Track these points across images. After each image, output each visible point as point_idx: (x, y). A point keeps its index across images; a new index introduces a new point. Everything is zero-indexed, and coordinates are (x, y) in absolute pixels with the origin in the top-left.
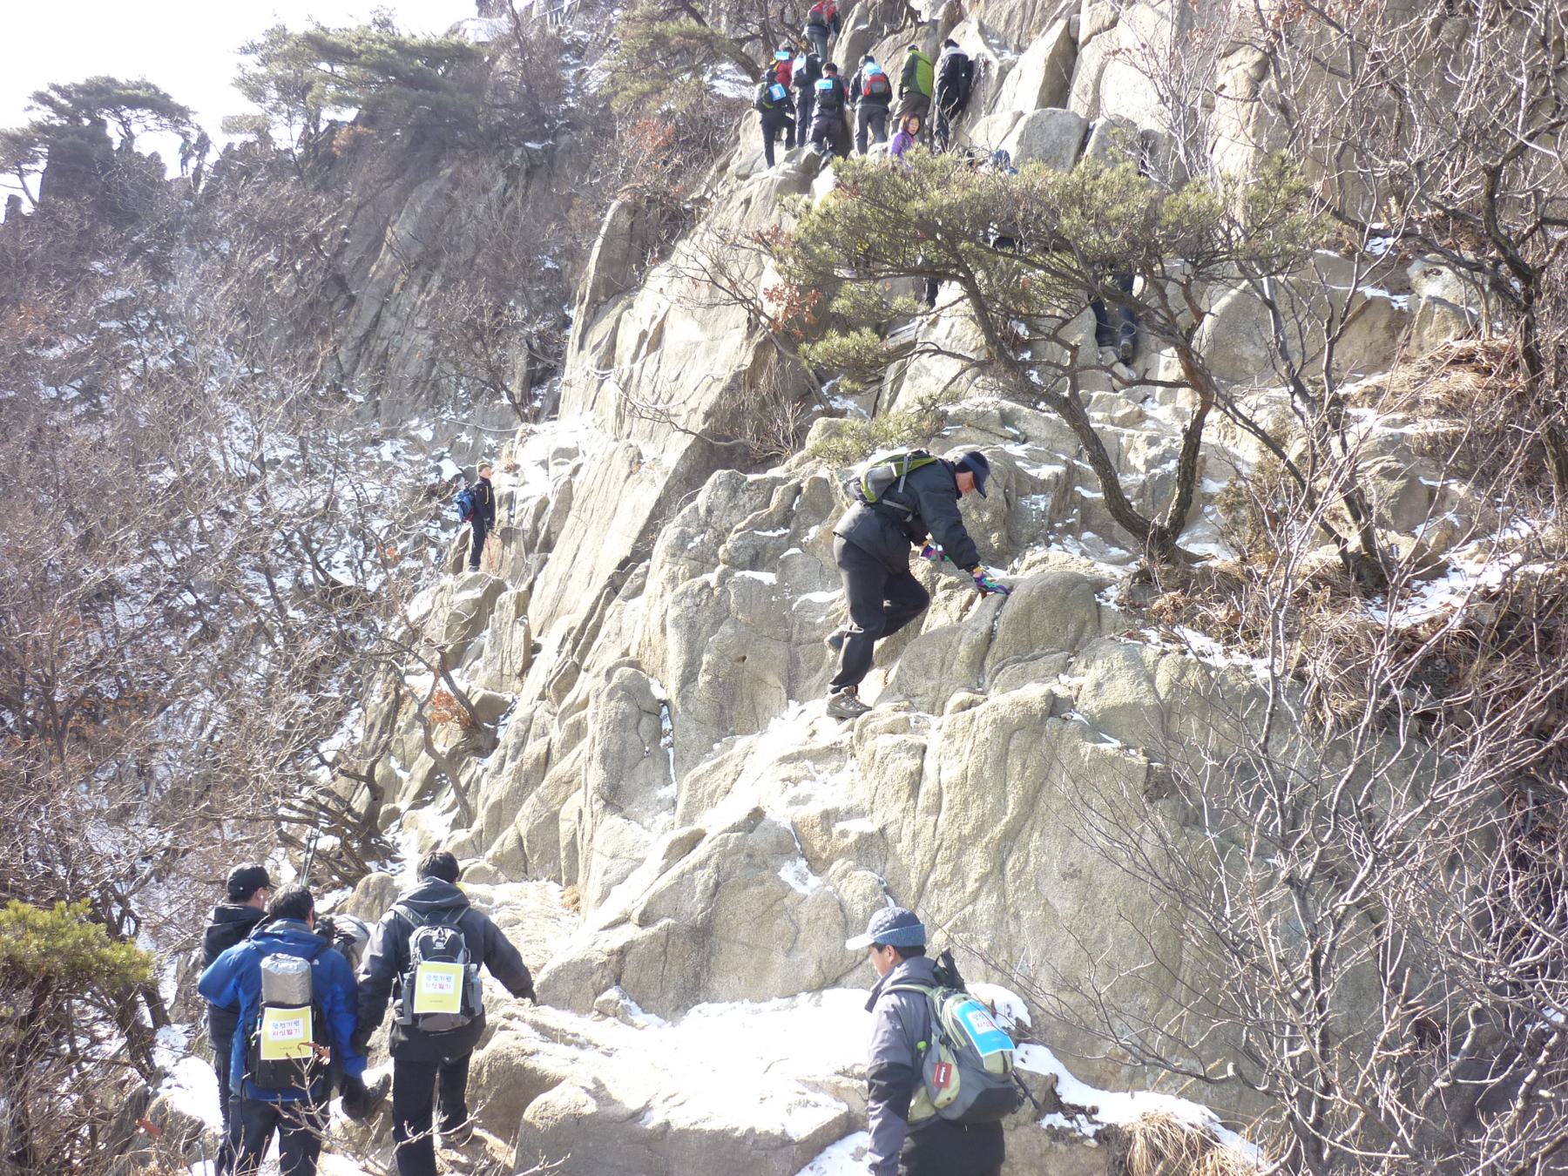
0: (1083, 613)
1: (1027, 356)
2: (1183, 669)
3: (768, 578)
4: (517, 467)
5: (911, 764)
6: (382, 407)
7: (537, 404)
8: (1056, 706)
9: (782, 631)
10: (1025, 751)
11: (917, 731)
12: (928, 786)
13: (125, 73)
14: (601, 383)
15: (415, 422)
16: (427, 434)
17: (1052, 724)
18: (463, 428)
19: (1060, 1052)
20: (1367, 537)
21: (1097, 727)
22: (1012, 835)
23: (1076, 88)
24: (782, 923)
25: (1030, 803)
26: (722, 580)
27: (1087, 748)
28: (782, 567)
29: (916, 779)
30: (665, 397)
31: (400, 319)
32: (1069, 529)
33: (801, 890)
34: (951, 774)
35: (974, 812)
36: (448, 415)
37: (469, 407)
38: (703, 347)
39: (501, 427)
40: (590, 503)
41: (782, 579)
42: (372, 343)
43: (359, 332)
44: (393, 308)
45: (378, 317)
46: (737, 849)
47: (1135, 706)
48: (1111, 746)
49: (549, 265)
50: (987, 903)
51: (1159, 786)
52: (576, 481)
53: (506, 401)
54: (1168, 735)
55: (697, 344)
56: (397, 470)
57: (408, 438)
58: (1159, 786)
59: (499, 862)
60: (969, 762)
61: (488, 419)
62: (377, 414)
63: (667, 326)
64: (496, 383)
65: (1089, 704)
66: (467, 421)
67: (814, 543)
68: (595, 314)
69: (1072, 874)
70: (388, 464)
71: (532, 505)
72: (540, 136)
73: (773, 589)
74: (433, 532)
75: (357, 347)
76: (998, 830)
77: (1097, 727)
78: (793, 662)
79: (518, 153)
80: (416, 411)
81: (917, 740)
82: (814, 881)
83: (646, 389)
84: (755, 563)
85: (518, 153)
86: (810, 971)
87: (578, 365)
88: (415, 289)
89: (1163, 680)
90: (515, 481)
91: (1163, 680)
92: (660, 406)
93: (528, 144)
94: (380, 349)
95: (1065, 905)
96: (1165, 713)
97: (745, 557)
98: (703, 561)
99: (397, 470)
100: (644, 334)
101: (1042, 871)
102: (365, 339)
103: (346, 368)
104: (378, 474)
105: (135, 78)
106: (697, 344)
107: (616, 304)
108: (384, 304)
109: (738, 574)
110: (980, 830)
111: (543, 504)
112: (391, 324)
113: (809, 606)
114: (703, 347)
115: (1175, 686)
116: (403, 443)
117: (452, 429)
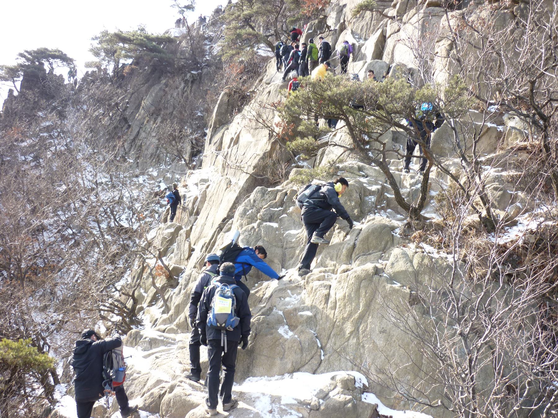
0: (387, 238)
1: (368, 147)
2: (423, 258)
3: (275, 225)
4: (187, 185)
5: (326, 292)
6: (139, 164)
7: (194, 163)
8: (377, 271)
9: (280, 244)
10: (366, 287)
11: (328, 280)
12: (331, 299)
13: (51, 47)
14: (217, 156)
15: (151, 169)
16: (155, 174)
17: (376, 278)
18: (168, 172)
19: (379, 396)
20: (488, 210)
21: (392, 279)
22: (362, 318)
23: (385, 53)
24: (279, 349)
25: (368, 306)
26: (259, 226)
27: (388, 286)
28: (280, 221)
29: (327, 297)
30: (239, 161)
31: (146, 133)
32: (382, 208)
33: (286, 337)
34: (340, 295)
35: (348, 309)
36: (163, 167)
37: (170, 164)
38: (253, 143)
39: (181, 171)
40: (213, 198)
41: (280, 226)
42: (136, 141)
43: (132, 138)
44: (144, 129)
45: (138, 132)
46: (263, 322)
47: (405, 272)
48: (397, 286)
49: (199, 114)
50: (353, 341)
51: (414, 300)
52: (208, 190)
53: (183, 162)
54: (417, 281)
55: (251, 142)
56: (144, 186)
57: (148, 175)
58: (414, 300)
59: (178, 326)
60: (347, 291)
61: (177, 168)
62: (138, 166)
63: (240, 136)
64: (180, 156)
65: (389, 270)
66: (169, 169)
67: (292, 213)
68: (215, 131)
69: (383, 331)
70: (141, 184)
71: (192, 199)
72: (197, 69)
73: (277, 229)
74: (157, 208)
75: (131, 143)
76: (356, 315)
77: (392, 279)
78: (284, 255)
79: (189, 75)
80: (151, 166)
81: (326, 283)
82: (291, 333)
83: (233, 158)
84: (271, 220)
85: (189, 75)
86: (289, 366)
87: (209, 150)
88: (152, 122)
89: (416, 262)
90: (186, 190)
91: (416, 262)
92: (238, 164)
93: (192, 72)
94: (139, 144)
95: (380, 343)
96: (416, 274)
97: (267, 218)
98: (252, 219)
99: (144, 186)
100: (232, 139)
101: (373, 330)
102: (134, 140)
103: (127, 150)
104: (137, 188)
105: (54, 48)
106: (251, 142)
107: (222, 128)
108: (141, 128)
109: (265, 224)
110: (350, 315)
111: (196, 199)
112: (143, 135)
113: (289, 235)
114: (253, 143)
115: (420, 264)
116: (147, 177)
117: (164, 172)
